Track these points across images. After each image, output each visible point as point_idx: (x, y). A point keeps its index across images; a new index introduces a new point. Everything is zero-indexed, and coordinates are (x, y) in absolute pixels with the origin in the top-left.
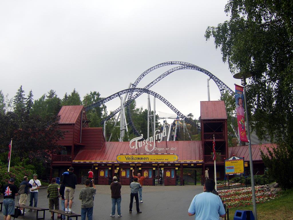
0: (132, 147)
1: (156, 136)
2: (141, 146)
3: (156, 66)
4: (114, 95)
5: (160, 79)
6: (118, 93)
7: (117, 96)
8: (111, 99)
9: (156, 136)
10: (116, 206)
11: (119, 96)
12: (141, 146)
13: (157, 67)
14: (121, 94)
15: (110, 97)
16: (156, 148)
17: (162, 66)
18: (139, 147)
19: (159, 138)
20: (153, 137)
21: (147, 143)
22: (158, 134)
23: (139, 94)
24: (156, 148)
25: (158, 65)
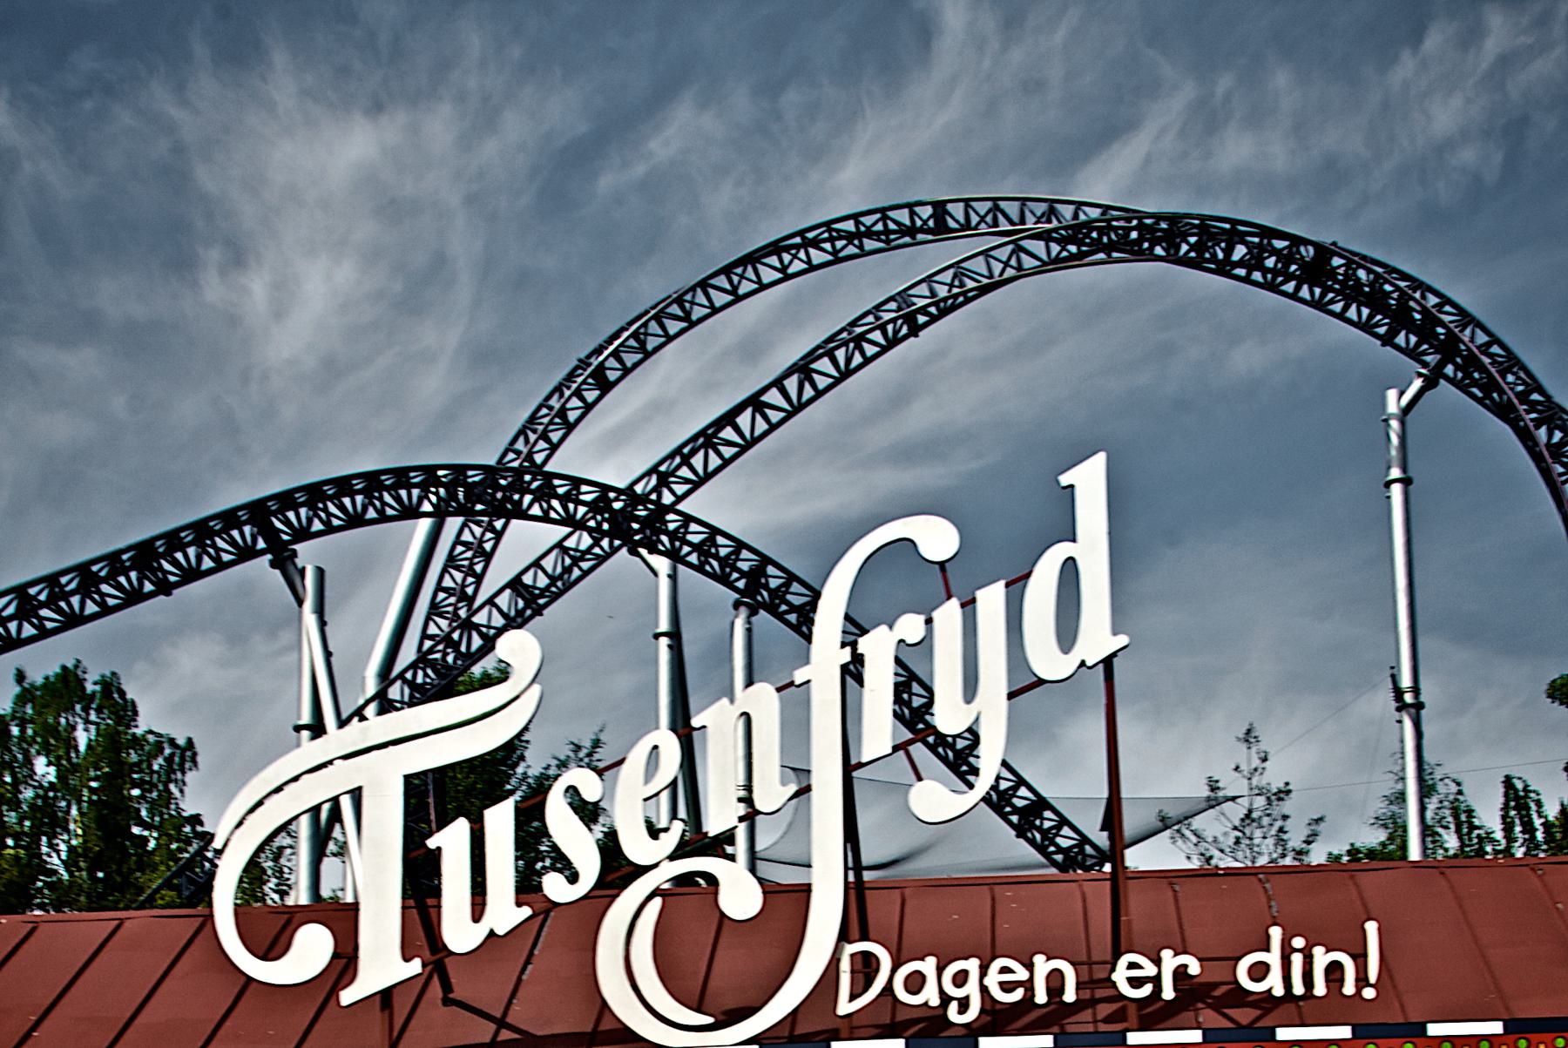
0: (272, 947)
1: (853, 671)
2: (505, 913)
3: (704, 285)
4: (202, 531)
5: (761, 426)
6: (258, 512)
7: (246, 553)
8: (165, 588)
9: (853, 671)
10: (785, 1040)
11: (283, 560)
12: (505, 913)
13: (720, 299)
14: (303, 534)
15: (145, 555)
16: (866, 968)
17: (768, 275)
18: (460, 933)
19: (949, 717)
20: (794, 694)
21: (637, 847)
22: (910, 627)
23: (543, 582)
24: (866, 968)
25: (727, 271)
